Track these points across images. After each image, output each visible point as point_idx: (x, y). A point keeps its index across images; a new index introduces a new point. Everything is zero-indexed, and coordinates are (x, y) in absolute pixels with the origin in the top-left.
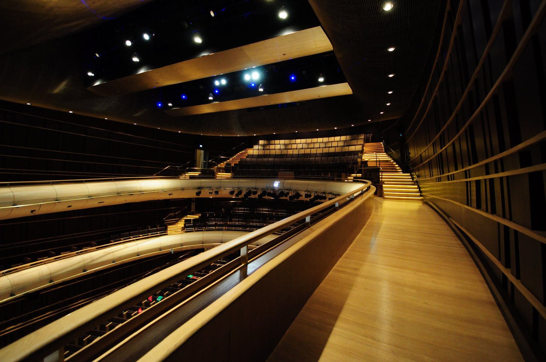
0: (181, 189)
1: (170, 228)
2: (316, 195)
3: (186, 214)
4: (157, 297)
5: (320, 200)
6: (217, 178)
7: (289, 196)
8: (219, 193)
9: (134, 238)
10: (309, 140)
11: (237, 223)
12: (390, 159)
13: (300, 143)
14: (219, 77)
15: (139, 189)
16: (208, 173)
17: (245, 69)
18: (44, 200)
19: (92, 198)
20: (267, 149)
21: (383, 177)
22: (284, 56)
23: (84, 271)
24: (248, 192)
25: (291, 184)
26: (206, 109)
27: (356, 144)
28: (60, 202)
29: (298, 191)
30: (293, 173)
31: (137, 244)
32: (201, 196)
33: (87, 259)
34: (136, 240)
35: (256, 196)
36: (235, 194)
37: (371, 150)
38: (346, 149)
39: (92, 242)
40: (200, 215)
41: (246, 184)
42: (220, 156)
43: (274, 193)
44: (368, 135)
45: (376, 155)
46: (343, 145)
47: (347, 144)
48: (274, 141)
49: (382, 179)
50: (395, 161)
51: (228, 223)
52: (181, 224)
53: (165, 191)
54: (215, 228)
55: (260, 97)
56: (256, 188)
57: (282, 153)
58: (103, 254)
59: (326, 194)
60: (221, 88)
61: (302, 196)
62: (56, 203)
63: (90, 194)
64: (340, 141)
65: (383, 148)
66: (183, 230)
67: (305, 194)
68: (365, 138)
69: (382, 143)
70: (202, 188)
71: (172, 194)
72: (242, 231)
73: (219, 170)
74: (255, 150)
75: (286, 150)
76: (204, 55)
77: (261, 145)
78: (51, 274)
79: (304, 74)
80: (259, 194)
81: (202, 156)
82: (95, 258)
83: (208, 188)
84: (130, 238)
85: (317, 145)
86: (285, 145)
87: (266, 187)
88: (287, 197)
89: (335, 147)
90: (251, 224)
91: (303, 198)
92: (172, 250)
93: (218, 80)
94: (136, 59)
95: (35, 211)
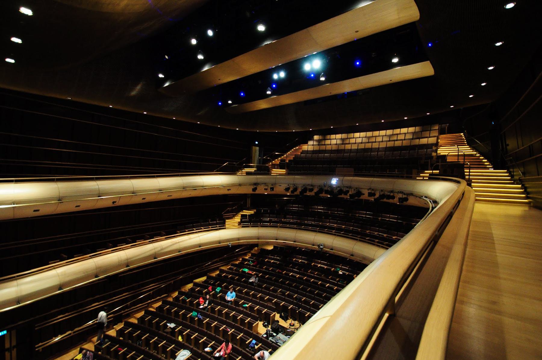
0: (238, 184)
1: (228, 222)
2: (381, 194)
3: (241, 210)
4: (216, 288)
5: (386, 199)
6: (272, 174)
7: (350, 195)
8: (275, 189)
9: (196, 230)
10: (369, 134)
11: (292, 220)
12: (475, 153)
13: (360, 137)
14: (277, 69)
15: (202, 184)
16: (263, 170)
17: (305, 56)
18: (123, 193)
19: (162, 192)
20: (323, 145)
21: (470, 174)
22: (358, 33)
23: (155, 258)
24: (304, 189)
25: (352, 181)
26: (262, 105)
27: (428, 136)
28: (137, 195)
29: (360, 190)
30: (353, 170)
31: (199, 236)
32: (257, 192)
33: (157, 248)
34: (199, 232)
35: (312, 193)
36: (290, 191)
37: (449, 142)
38: (417, 142)
39: (162, 232)
40: (255, 211)
41: (301, 180)
42: (274, 153)
43: (331, 190)
44: (443, 125)
45: (458, 148)
46: (412, 137)
47: (417, 136)
48: (329, 135)
49: (470, 177)
50: (482, 154)
51: (283, 220)
52: (238, 219)
53: (224, 187)
54: (270, 224)
55: (320, 87)
56: (312, 185)
57: (339, 149)
58: (171, 244)
59: (395, 194)
60: (280, 82)
61: (364, 194)
62: (132, 195)
63: (161, 188)
64: (408, 133)
65: (465, 140)
66: (240, 225)
67: (369, 193)
68: (440, 129)
69: (462, 134)
70: (258, 184)
71: (230, 190)
72: (296, 229)
73: (274, 166)
74: (310, 146)
75: (344, 145)
76: (266, 43)
77: (316, 141)
78: (127, 259)
79: (373, 56)
80: (315, 191)
81: (257, 153)
82: (164, 247)
83: (263, 184)
84: (194, 230)
85: (379, 139)
86: (343, 140)
87: (323, 184)
88: (347, 195)
89: (402, 140)
90: (306, 222)
91: (365, 196)
92: (230, 243)
93: (276, 72)
94: (200, 57)
95: (115, 202)
